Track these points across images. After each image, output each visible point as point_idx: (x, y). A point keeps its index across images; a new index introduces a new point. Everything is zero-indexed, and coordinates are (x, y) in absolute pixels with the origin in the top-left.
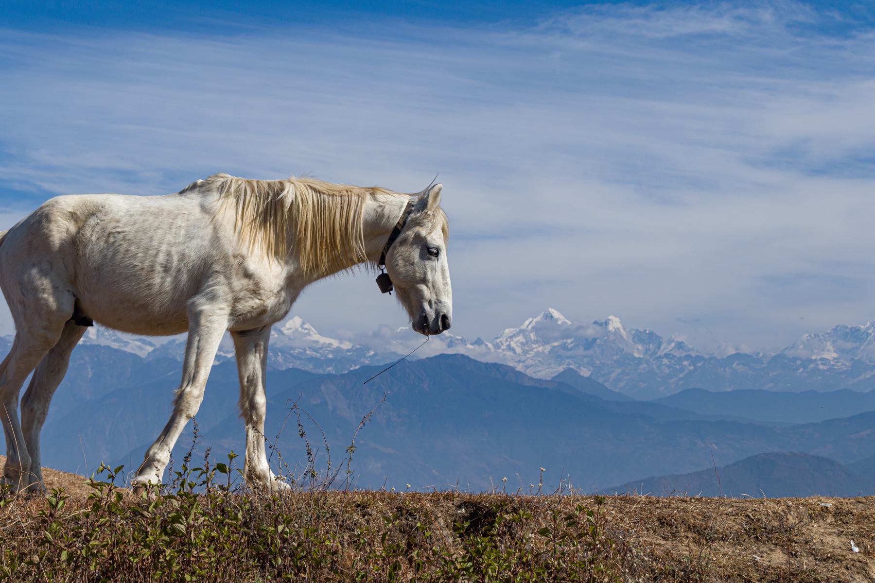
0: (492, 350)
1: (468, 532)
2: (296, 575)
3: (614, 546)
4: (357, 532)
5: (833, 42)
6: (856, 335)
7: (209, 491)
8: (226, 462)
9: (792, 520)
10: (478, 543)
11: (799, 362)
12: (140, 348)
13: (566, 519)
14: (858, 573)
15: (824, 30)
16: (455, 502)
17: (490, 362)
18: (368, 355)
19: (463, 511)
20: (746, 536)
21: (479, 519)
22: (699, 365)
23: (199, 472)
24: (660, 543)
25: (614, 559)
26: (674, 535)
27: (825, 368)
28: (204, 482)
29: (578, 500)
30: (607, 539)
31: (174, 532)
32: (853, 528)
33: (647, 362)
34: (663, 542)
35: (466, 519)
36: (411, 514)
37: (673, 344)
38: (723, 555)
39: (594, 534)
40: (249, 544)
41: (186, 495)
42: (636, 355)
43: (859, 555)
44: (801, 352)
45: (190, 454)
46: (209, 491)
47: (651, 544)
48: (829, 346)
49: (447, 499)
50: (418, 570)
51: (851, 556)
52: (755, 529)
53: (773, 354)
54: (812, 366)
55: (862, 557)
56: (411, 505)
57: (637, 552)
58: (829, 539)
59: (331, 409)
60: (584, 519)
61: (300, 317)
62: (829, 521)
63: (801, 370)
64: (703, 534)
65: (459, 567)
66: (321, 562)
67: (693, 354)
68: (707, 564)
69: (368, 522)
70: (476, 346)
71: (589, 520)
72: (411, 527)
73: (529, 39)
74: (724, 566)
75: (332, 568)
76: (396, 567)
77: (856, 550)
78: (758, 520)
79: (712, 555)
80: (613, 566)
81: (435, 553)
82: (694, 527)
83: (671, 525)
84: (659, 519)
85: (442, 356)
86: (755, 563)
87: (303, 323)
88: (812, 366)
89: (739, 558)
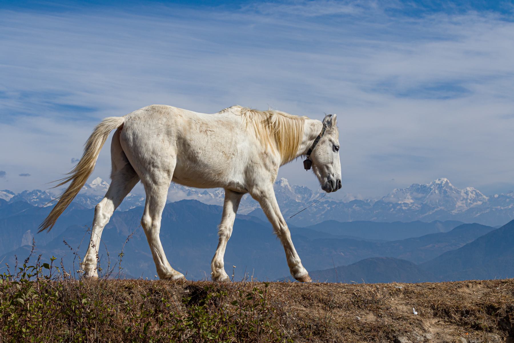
0: (213, 198)
1: (190, 303)
2: (89, 328)
3: (275, 311)
4: (126, 303)
5: (412, 20)
6: (423, 189)
7: (38, 279)
8: (49, 262)
9: (379, 296)
10: (196, 310)
11: (391, 205)
12: (6, 195)
13: (247, 295)
14: (417, 327)
15: (407, 13)
16: (183, 286)
17: (212, 204)
18: (140, 200)
19: (188, 291)
20: (352, 306)
21: (197, 296)
22: (334, 206)
23: (32, 268)
24: (303, 310)
25: (275, 318)
26: (311, 305)
27: (406, 208)
28: (35, 274)
29: (256, 285)
30: (271, 307)
31: (17, 304)
32: (414, 300)
33: (303, 205)
34: (304, 309)
35: (189, 295)
36: (157, 293)
37: (318, 195)
38: (339, 316)
39: (263, 305)
40: (62, 311)
41: (26, 281)
42: (297, 201)
43: (417, 316)
44: (392, 199)
45: (28, 259)
46: (38, 279)
47: (297, 310)
48: (408, 196)
49: (179, 284)
50: (161, 325)
51: (413, 317)
52: (358, 301)
53: (376, 200)
54: (398, 207)
55: (419, 317)
56: (157, 288)
57: (289, 315)
58: (400, 307)
59: (118, 231)
60: (259, 296)
61: (101, 178)
62: (401, 297)
63: (392, 209)
64: (328, 304)
65: (185, 324)
66: (104, 320)
67: (330, 200)
68: (329, 321)
69: (132, 297)
70: (204, 195)
71: (260, 296)
72: (157, 300)
73: (236, 16)
74: (339, 323)
75: (110, 324)
76: (149, 324)
77: (416, 313)
78: (360, 296)
79: (333, 316)
80: (275, 323)
81: (171, 316)
82: (322, 300)
83: (309, 299)
84: (302, 296)
85: (184, 201)
86: (358, 321)
87: (103, 181)
88: (398, 207)
89: (348, 318)
